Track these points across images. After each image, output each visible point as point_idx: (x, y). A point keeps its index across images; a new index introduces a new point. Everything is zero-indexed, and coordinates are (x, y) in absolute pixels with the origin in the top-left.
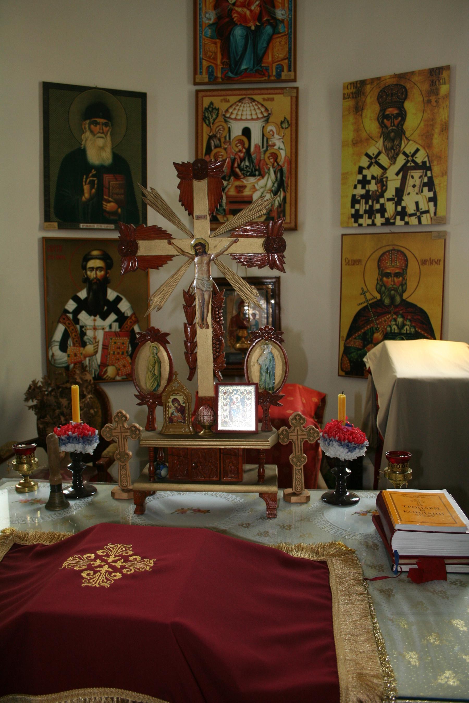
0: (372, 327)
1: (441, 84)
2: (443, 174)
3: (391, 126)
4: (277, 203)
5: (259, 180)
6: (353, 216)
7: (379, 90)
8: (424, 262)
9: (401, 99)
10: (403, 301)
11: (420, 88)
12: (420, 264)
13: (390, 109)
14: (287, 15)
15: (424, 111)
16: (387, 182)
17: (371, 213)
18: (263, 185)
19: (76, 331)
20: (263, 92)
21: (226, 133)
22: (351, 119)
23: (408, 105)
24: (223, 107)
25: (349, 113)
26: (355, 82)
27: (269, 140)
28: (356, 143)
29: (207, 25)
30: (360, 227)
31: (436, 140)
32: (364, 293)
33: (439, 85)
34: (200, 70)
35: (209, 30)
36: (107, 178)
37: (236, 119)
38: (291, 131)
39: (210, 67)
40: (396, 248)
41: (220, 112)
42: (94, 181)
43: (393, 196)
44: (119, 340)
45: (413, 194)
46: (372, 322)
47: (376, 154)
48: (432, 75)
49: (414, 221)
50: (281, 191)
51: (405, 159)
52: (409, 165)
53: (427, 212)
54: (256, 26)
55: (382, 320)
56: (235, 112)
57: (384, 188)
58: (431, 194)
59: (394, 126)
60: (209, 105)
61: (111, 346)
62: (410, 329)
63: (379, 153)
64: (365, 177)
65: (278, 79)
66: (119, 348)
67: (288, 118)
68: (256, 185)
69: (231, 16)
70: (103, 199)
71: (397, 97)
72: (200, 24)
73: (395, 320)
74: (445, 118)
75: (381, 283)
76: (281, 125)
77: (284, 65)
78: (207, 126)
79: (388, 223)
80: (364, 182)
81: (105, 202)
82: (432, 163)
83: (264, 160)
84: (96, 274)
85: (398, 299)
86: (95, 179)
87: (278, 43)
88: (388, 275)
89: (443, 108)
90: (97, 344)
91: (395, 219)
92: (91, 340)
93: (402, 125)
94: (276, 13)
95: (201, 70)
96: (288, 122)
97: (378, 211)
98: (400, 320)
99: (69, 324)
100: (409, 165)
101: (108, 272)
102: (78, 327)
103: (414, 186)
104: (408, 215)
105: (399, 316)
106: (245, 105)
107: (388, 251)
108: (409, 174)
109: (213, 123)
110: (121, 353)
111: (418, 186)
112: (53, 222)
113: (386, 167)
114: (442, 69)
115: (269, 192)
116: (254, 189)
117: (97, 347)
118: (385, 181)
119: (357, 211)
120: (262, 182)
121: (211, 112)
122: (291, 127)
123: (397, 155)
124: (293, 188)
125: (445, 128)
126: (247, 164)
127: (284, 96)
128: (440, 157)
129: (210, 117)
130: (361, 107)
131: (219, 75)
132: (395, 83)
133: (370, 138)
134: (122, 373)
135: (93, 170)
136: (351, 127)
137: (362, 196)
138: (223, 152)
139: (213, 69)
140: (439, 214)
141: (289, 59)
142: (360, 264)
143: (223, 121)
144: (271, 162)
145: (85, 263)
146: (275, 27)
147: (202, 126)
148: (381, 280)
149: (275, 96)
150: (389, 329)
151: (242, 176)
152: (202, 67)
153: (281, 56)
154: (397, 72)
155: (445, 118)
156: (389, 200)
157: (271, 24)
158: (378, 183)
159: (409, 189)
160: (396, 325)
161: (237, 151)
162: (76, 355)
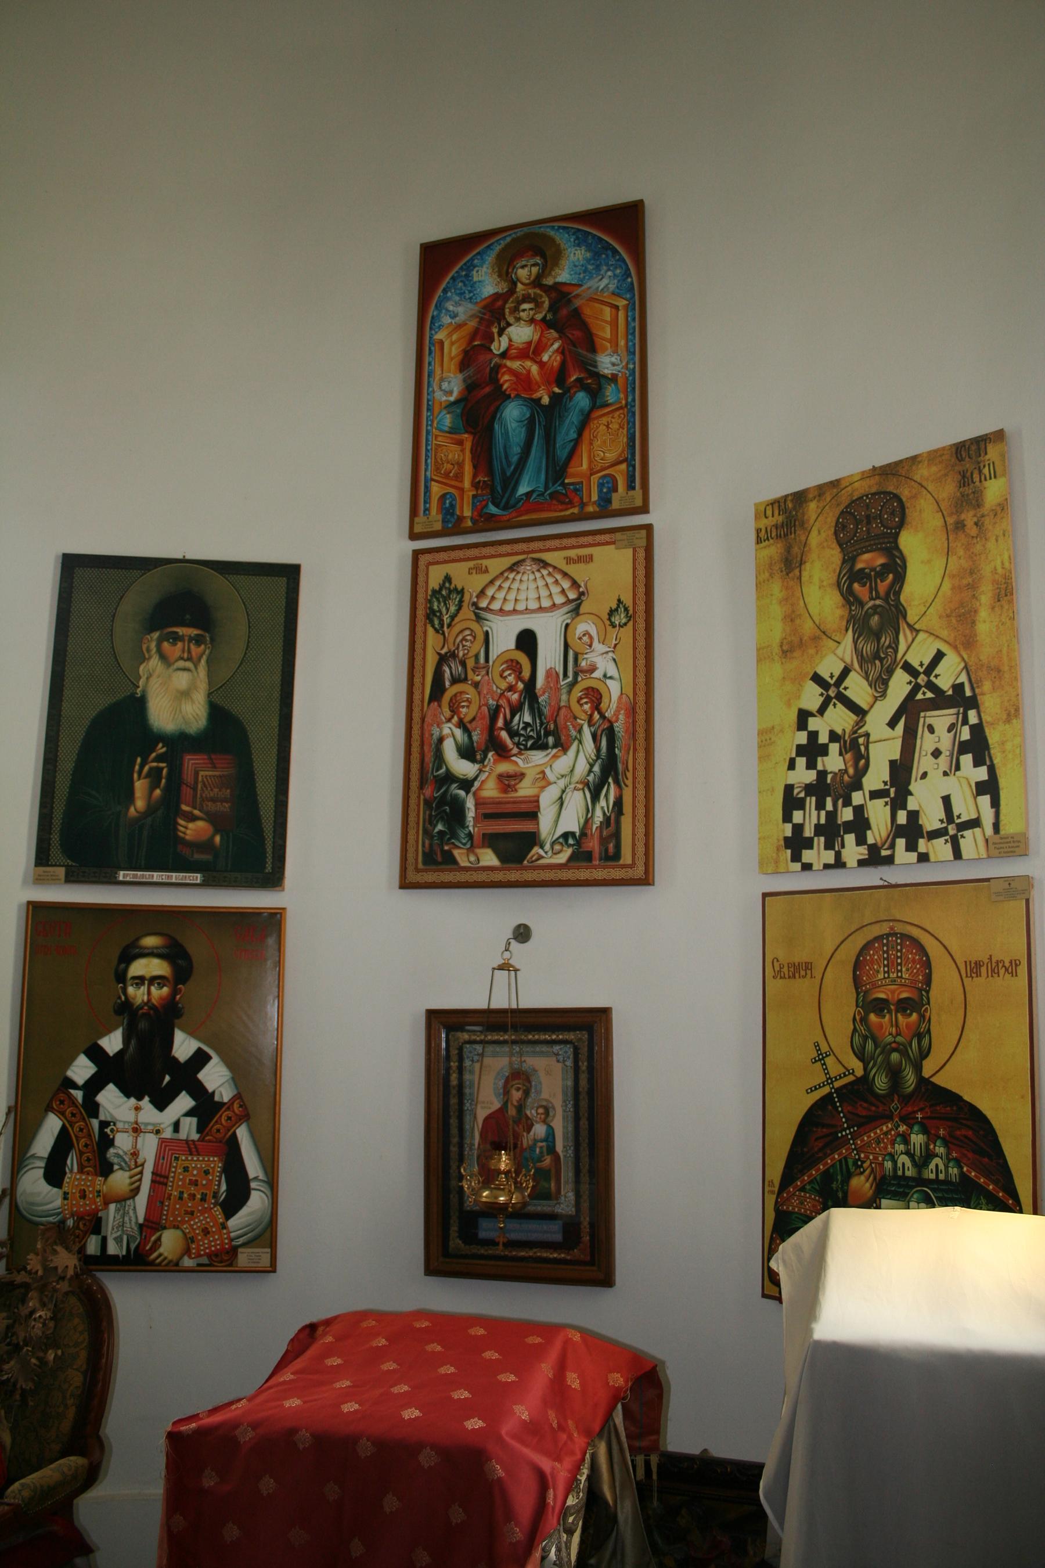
0: (846, 1158)
1: (986, 480)
2: (1009, 715)
3: (871, 599)
4: (598, 817)
5: (555, 757)
6: (788, 842)
7: (837, 512)
8: (975, 968)
9: (891, 529)
10: (923, 1083)
11: (936, 497)
12: (964, 975)
13: (866, 556)
14: (624, 364)
16: (867, 748)
17: (831, 832)
18: (565, 770)
19: (89, 1136)
20: (566, 542)
21: (478, 647)
22: (776, 588)
23: (909, 542)
24: (472, 584)
25: (771, 575)
26: (782, 497)
27: (580, 656)
28: (788, 650)
29: (443, 405)
30: (807, 873)
31: (985, 625)
32: (820, 1058)
33: (980, 481)
34: (425, 506)
35: (448, 416)
36: (191, 762)
37: (501, 611)
38: (635, 630)
39: (448, 496)
40: (899, 928)
41: (466, 597)
42: (162, 769)
43: (885, 783)
44: (197, 1163)
45: (935, 775)
46: (845, 1141)
47: (837, 674)
48: (960, 459)
49: (940, 849)
50: (609, 784)
51: (910, 683)
52: (920, 696)
53: (975, 823)
54: (553, 397)
55: (869, 1136)
56: (500, 595)
57: (863, 762)
59: (878, 597)
60: (441, 582)
61: (174, 1177)
62: (946, 1167)
63: (846, 672)
64: (813, 736)
65: (605, 510)
66: (195, 1183)
67: (628, 600)
68: (548, 771)
69: (498, 380)
70: (178, 812)
71: (881, 522)
72: (428, 405)
73: (906, 1140)
74: (1003, 563)
75: (862, 1029)
76: (609, 619)
77: (616, 476)
78: (437, 631)
79: (875, 858)
80: (812, 751)
81: (184, 820)
82: (978, 687)
83: (569, 707)
84: (149, 993)
85: (910, 1078)
86: (164, 765)
87: (603, 428)
88: (880, 1006)
89: (997, 540)
90: (139, 1169)
91: (892, 846)
92: (124, 1160)
93: (898, 594)
94: (599, 364)
95: (428, 505)
96: (626, 609)
97: (848, 827)
98: (917, 1139)
99: (73, 1115)
100: (920, 696)
101: (180, 990)
102: (95, 1123)
104: (925, 835)
105: (916, 1128)
106: (525, 578)
107: (878, 938)
108: (921, 720)
109: (449, 626)
110: (199, 1196)
111: (948, 753)
112: (55, 865)
113: (864, 706)
114: (986, 440)
115: (580, 786)
116: (543, 780)
117: (138, 1177)
118: (863, 744)
119: (798, 829)
120: (563, 763)
121: (446, 599)
122: (635, 622)
123: (890, 672)
124: (641, 774)
126: (527, 718)
127: (617, 548)
128: (999, 671)
129: (444, 610)
130: (799, 559)
131: (467, 513)
132: (873, 490)
133: (823, 633)
134: (198, 1250)
135: (160, 745)
136: (777, 611)
137: (809, 789)
138: (471, 693)
139: (454, 499)
140: (1007, 828)
141: (629, 461)
142: (809, 975)
143: (474, 618)
144: (585, 712)
145: (123, 966)
146: (595, 393)
147: (425, 633)
148: (864, 1020)
149: (594, 551)
150: (888, 1165)
151: (515, 751)
152: (430, 497)
153: (611, 456)
154: (878, 464)
155: (1003, 563)
156: (875, 795)
157: (586, 388)
158: (846, 753)
159: (923, 762)
160: (907, 1153)
161: (503, 688)
162: (83, 1195)
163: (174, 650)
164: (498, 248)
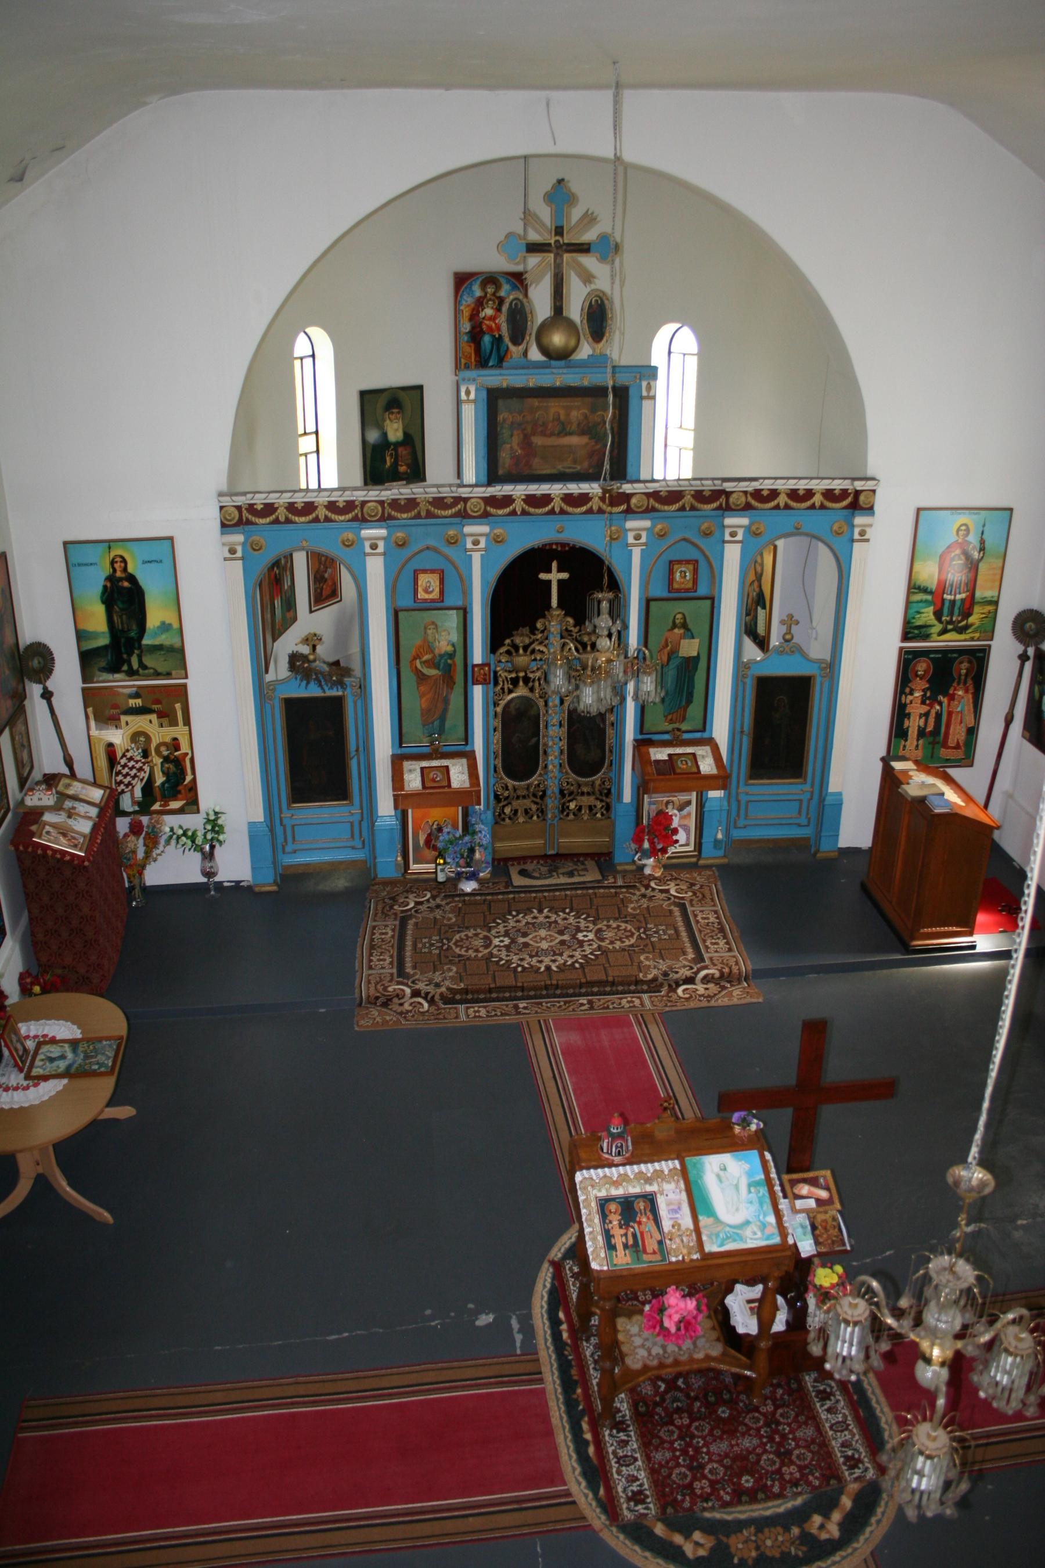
36: (400, 450)
163: (393, 417)
164: (480, 279)
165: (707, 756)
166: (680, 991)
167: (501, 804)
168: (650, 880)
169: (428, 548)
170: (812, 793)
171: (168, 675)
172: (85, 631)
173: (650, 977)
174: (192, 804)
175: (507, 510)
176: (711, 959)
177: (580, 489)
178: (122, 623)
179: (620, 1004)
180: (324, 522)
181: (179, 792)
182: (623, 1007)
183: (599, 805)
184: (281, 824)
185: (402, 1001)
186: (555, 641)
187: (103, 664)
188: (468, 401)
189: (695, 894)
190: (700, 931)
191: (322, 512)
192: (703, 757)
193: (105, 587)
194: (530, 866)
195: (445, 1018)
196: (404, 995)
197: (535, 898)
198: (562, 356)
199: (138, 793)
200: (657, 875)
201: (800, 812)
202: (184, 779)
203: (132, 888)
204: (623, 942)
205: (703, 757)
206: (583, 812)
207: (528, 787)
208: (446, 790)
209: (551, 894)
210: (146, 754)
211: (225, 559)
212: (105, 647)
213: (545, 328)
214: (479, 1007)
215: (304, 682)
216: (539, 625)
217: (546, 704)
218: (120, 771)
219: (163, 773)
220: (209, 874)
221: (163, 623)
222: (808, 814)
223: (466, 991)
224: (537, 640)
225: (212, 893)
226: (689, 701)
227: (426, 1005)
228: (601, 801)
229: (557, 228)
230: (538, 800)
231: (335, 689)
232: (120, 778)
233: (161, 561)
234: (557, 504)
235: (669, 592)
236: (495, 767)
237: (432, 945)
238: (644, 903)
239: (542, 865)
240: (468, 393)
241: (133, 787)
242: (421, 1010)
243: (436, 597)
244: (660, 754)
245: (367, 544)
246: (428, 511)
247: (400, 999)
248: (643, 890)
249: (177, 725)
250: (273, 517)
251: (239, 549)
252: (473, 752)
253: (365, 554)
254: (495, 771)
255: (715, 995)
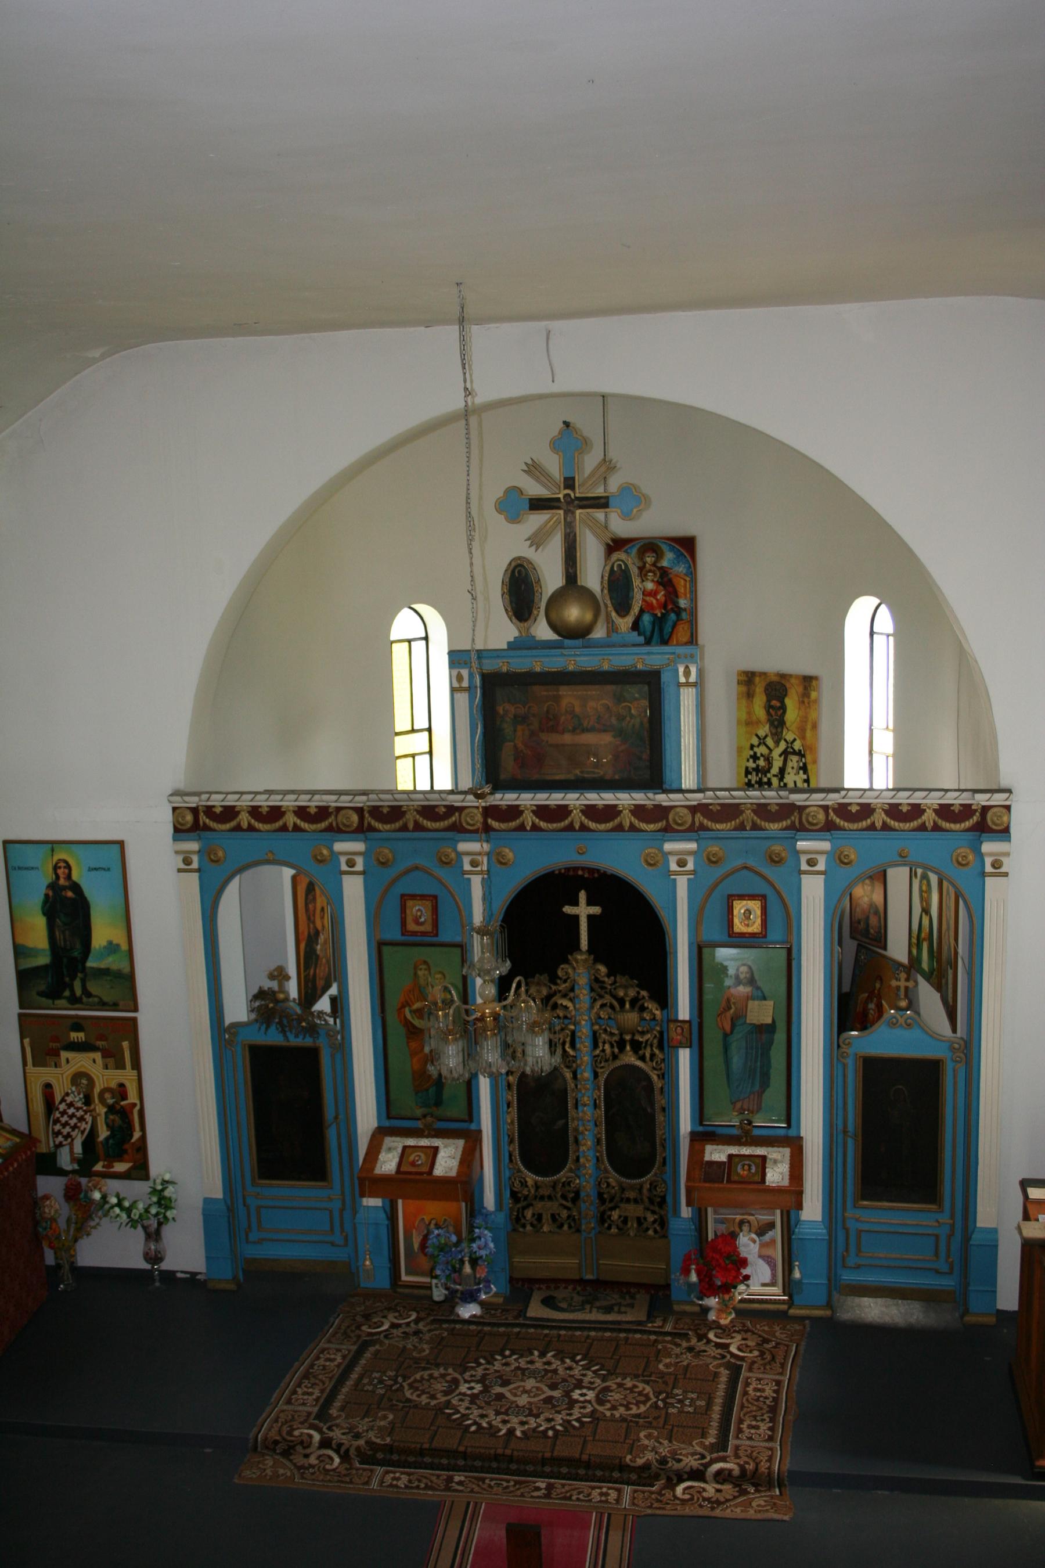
15: (799, 709)
22: (744, 702)
31: (809, 734)
54: (662, 614)
58: (805, 777)
63: (766, 736)
80: (755, 757)
93: (783, 717)
97: (766, 783)
103: (793, 768)
125: (815, 726)
133: (758, 722)
137: (754, 769)
156: (774, 776)
159: (789, 769)
165: (782, 1162)
166: (679, 1489)
167: (519, 1205)
168: (711, 1329)
169: (746, 868)
170: (952, 1226)
171: (115, 1007)
172: (23, 946)
173: (640, 1462)
174: (140, 1170)
175: (513, 824)
176: (737, 1448)
177: (603, 799)
178: (65, 941)
179: (589, 1495)
180: (628, 831)
181: (125, 1151)
182: (590, 1501)
183: (651, 1218)
184: (245, 1205)
185: (308, 1451)
186: (584, 995)
187: (43, 987)
188: (688, 684)
189: (762, 1354)
190: (742, 1407)
191: (410, 818)
192: (775, 1162)
193: (47, 896)
194: (560, 1294)
195: (351, 1482)
196: (311, 1443)
197: (546, 1335)
198: (577, 633)
199: (78, 1149)
200: (723, 1322)
201: (937, 1254)
202: (131, 1136)
203: (58, 1267)
204: (628, 1408)
205: (775, 1162)
206: (629, 1224)
207: (554, 1186)
208: (761, 1187)
209: (570, 1333)
210: (88, 1100)
211: (180, 871)
212: (45, 967)
213: (558, 598)
214: (609, 1488)
215: (264, 1027)
216: (560, 973)
217: (575, 1077)
218: (58, 1118)
219: (108, 1125)
220: (155, 1258)
221: (110, 943)
222: (948, 1256)
223: (390, 1449)
224: (560, 991)
225: (157, 1284)
226: (765, 1083)
227: (337, 1460)
228: (654, 1212)
229: (566, 479)
230: (569, 1204)
231: (301, 1037)
232: (58, 1127)
233: (109, 869)
234: (577, 817)
235: (403, 934)
236: (510, 1155)
237: (680, 1401)
238: (687, 1359)
239: (578, 1293)
240: (687, 673)
241: (73, 1140)
242: (328, 1467)
243: (756, 931)
244: (717, 1154)
245: (343, 860)
246: (416, 822)
247: (305, 1448)
248: (694, 1341)
249: (124, 1068)
250: (233, 824)
251: (195, 859)
252: (480, 1132)
253: (801, 872)
254: (511, 1160)
255: (727, 1500)
